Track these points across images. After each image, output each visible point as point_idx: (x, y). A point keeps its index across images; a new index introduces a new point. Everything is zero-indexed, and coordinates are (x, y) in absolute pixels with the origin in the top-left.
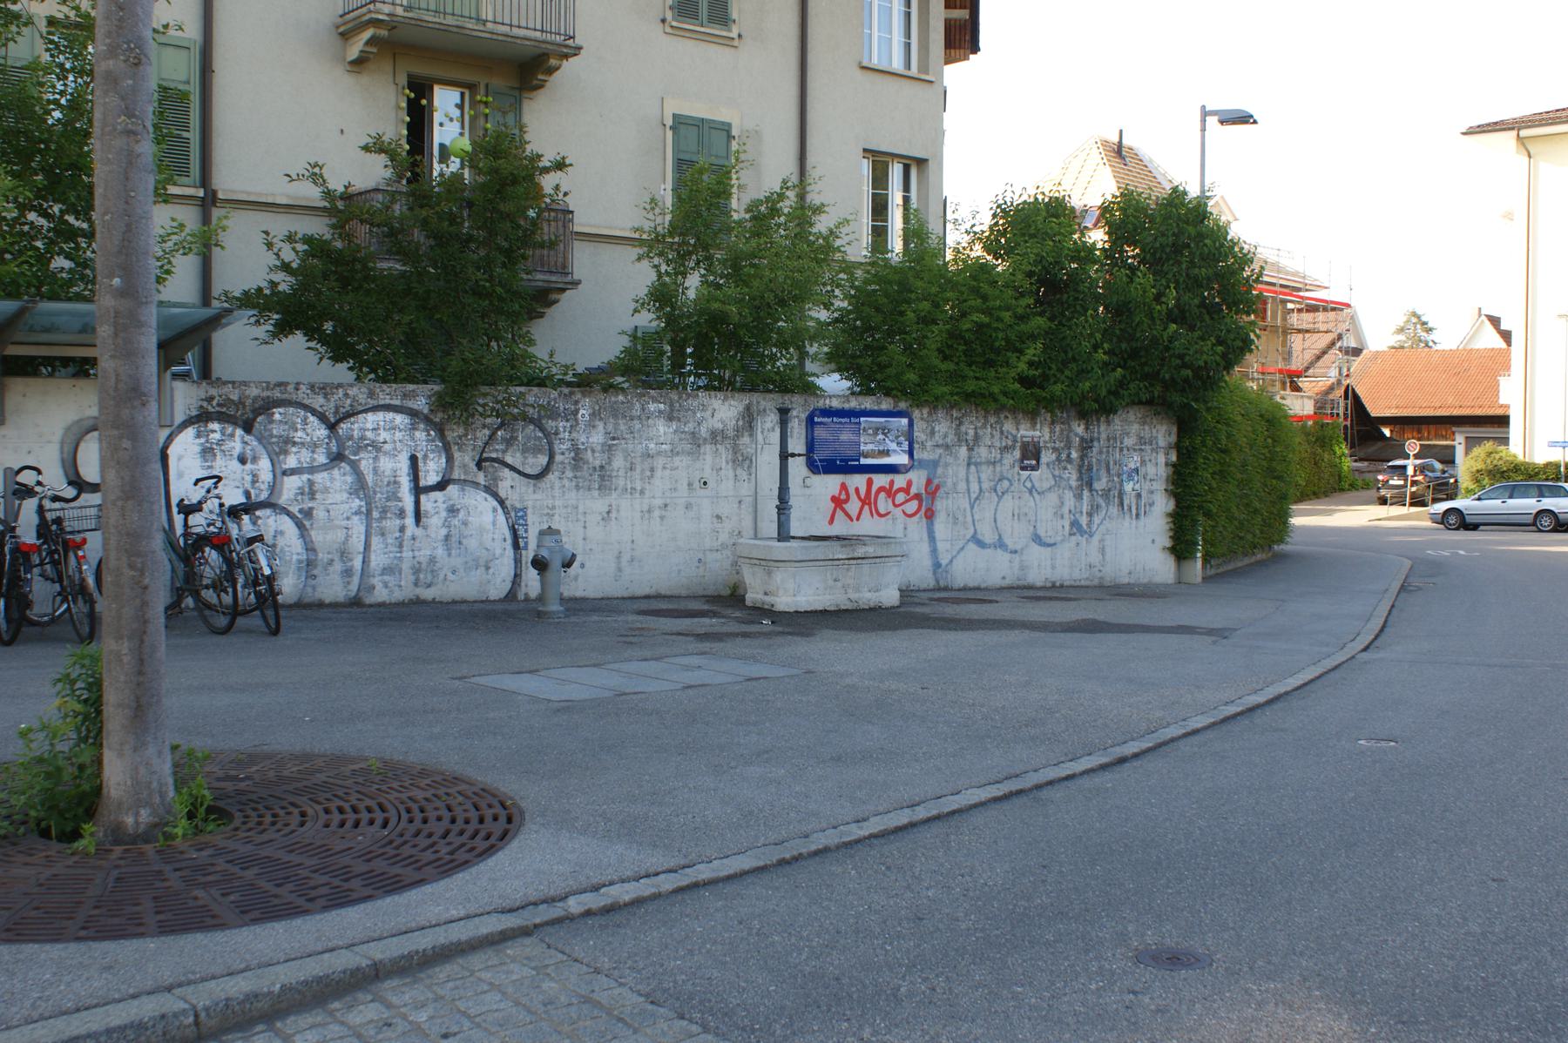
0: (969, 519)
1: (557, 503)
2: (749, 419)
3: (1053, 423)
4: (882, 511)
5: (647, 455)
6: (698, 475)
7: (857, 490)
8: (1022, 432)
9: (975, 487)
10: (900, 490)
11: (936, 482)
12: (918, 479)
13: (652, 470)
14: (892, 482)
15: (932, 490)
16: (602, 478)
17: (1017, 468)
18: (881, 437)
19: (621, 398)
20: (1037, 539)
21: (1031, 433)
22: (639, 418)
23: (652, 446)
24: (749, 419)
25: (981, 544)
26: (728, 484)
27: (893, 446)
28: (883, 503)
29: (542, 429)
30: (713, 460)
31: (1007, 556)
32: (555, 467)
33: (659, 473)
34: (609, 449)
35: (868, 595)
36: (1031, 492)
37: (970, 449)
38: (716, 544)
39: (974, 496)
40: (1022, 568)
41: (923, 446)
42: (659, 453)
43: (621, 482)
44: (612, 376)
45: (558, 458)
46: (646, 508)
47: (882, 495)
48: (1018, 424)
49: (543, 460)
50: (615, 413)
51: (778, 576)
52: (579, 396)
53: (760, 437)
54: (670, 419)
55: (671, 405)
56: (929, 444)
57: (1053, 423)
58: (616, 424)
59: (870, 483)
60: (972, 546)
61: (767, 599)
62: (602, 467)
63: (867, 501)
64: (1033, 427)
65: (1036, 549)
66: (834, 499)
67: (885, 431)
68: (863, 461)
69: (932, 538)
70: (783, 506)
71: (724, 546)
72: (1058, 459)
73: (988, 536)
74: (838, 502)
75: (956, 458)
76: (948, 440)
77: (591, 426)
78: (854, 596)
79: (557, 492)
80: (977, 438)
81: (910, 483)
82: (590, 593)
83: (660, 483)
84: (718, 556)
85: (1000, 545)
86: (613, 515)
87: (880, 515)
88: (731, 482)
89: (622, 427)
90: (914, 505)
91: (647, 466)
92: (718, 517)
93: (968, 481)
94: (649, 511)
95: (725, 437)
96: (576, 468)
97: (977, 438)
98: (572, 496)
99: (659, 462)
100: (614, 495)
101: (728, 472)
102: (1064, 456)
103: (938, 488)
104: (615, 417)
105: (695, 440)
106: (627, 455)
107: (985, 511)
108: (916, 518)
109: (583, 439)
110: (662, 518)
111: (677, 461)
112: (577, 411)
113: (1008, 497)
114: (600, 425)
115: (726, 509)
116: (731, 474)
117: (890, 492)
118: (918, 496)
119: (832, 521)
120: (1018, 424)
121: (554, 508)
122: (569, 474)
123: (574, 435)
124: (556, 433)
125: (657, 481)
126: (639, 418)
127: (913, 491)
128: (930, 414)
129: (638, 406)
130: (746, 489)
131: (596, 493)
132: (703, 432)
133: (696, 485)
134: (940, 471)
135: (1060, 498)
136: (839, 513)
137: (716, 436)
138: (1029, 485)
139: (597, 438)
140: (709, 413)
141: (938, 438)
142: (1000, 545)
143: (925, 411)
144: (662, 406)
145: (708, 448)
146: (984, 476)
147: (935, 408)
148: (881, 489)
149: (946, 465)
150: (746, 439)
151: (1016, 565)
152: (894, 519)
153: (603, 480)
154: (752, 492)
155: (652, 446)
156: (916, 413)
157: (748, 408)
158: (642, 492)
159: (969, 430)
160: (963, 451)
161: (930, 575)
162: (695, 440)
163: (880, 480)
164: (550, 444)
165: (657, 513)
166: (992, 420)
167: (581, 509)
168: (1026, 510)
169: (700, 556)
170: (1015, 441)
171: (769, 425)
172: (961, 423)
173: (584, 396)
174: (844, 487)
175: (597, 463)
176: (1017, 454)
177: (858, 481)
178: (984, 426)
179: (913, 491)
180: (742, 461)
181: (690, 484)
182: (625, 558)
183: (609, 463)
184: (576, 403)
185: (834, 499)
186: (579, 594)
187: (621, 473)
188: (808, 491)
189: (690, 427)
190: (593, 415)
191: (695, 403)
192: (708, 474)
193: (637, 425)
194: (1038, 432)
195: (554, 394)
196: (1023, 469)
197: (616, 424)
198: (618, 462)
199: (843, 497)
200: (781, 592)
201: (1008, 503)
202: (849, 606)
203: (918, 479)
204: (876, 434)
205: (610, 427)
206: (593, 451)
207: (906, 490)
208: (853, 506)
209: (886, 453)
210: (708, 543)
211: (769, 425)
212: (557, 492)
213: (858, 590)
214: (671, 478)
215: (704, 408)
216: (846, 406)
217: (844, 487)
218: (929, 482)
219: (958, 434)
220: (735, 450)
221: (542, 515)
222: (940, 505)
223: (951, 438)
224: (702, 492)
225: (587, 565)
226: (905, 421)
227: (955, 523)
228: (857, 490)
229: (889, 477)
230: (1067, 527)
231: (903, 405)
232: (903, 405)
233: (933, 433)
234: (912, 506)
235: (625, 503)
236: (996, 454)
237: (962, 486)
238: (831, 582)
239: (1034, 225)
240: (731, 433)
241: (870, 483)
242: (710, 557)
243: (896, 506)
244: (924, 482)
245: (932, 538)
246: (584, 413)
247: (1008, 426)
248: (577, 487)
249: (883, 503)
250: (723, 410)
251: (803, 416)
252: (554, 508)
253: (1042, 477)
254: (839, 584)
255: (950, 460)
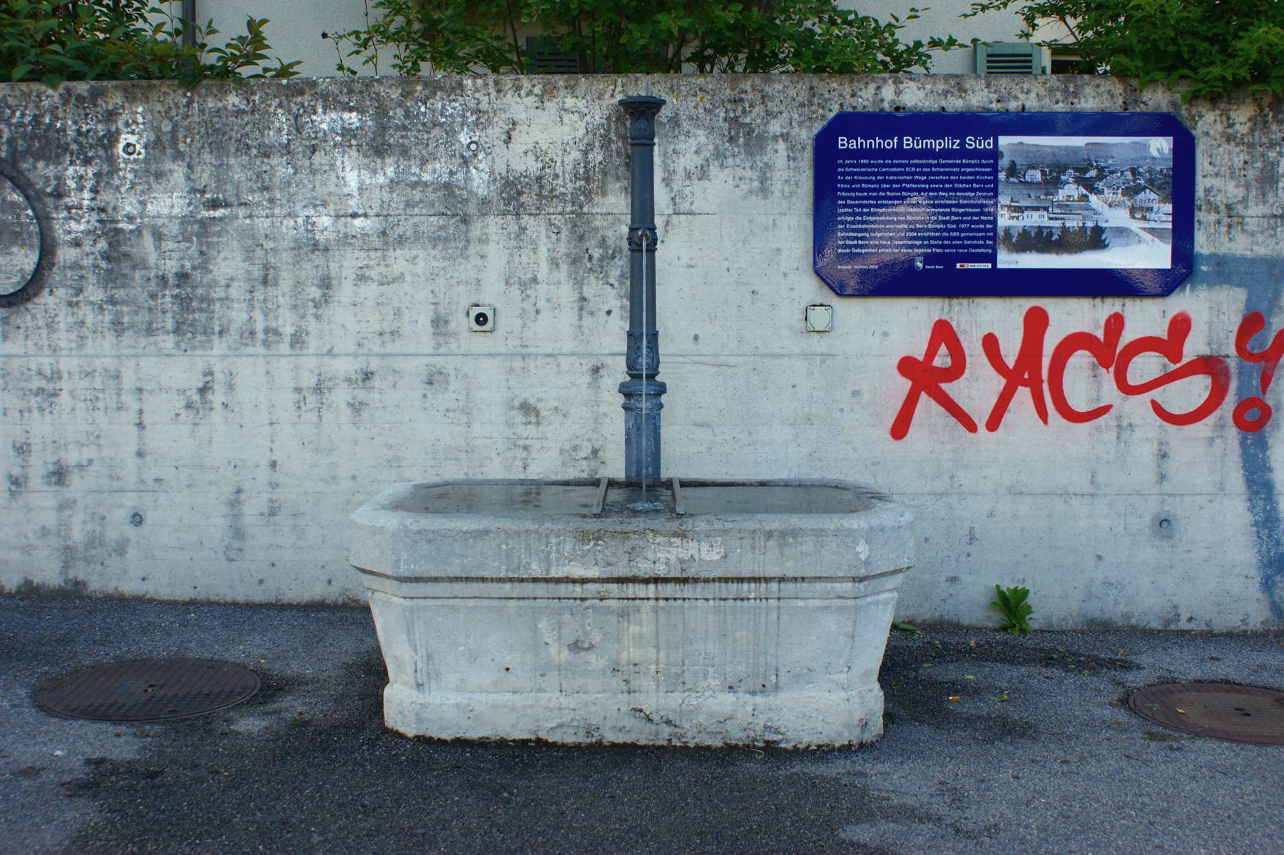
1: (66, 364)
4: (1079, 402)
5: (312, 246)
6: (463, 297)
7: (990, 344)
12: (1212, 315)
13: (326, 283)
14: (1115, 324)
16: (184, 303)
18: (1071, 191)
19: (233, 100)
22: (287, 149)
23: (325, 221)
27: (1117, 217)
28: (1083, 381)
29: (21, 185)
32: (56, 275)
33: (345, 291)
34: (200, 231)
35: (725, 702)
41: (1232, 216)
42: (346, 240)
43: (238, 315)
44: (105, 39)
45: (65, 255)
46: (309, 381)
47: (1081, 360)
49: (26, 259)
50: (217, 138)
52: (116, 99)
54: (378, 149)
55: (381, 113)
56: (1254, 211)
58: (221, 172)
59: (1036, 324)
62: (183, 277)
63: (1031, 373)
66: (907, 366)
67: (1090, 175)
68: (1007, 260)
74: (926, 377)
77: (152, 174)
78: (656, 700)
79: (64, 338)
81: (1181, 326)
82: (161, 588)
83: (348, 321)
86: (217, 397)
88: (568, 317)
89: (239, 175)
90: (1195, 390)
91: (309, 271)
92: (526, 408)
94: (318, 389)
96: (111, 279)
98: (105, 349)
99: (348, 263)
100: (219, 347)
104: (219, 148)
105: (456, 207)
106: (252, 244)
109: (129, 206)
110: (357, 407)
111: (399, 260)
112: (113, 138)
114: (178, 172)
115: (547, 386)
116: (566, 293)
117: (1109, 350)
118: (1209, 365)
119: (900, 429)
121: (56, 375)
122: (95, 293)
123: (106, 197)
124: (59, 194)
125: (340, 314)
126: (287, 149)
127: (1194, 347)
129: (282, 119)
131: (169, 342)
132: (479, 181)
133: (460, 323)
137: (514, 194)
139: (168, 204)
140: (496, 132)
143: (1242, 116)
144: (353, 118)
145: (493, 224)
153: (189, 306)
155: (325, 221)
156: (1207, 124)
158: (298, 340)
161: (1254, 590)
162: (456, 207)
163: (1071, 316)
164: (43, 220)
165: (341, 395)
167: (129, 379)
171: (688, 160)
173: (130, 97)
175: (171, 267)
179: (1194, 347)
181: (439, 323)
182: (252, 509)
183: (204, 267)
184: (111, 116)
185: (907, 366)
186: (131, 586)
187: (237, 291)
188: (819, 345)
189: (438, 170)
190: (156, 146)
191: (454, 108)
192: (492, 295)
193: (281, 168)
195: (51, 96)
197: (221, 172)
198: (229, 264)
199: (942, 359)
202: (641, 734)
203: (1212, 315)
204: (1052, 183)
205: (204, 176)
206: (158, 237)
207: (1171, 344)
208: (978, 388)
209: (1096, 239)
212: (64, 338)
213: (676, 680)
214: (387, 302)
215: (481, 118)
216: (955, 104)
217: (943, 333)
218: (1252, 323)
221: (25, 393)
224: (481, 343)
225: (150, 517)
226: (1160, 146)
229: (1109, 306)
231: (1157, 99)
232: (1157, 99)
235: (249, 369)
240: (566, 185)
241: (1036, 324)
244: (1233, 321)
246: (132, 140)
248: (118, 327)
249: (1083, 381)
251: (806, 135)
252: (56, 375)
254: (596, 661)
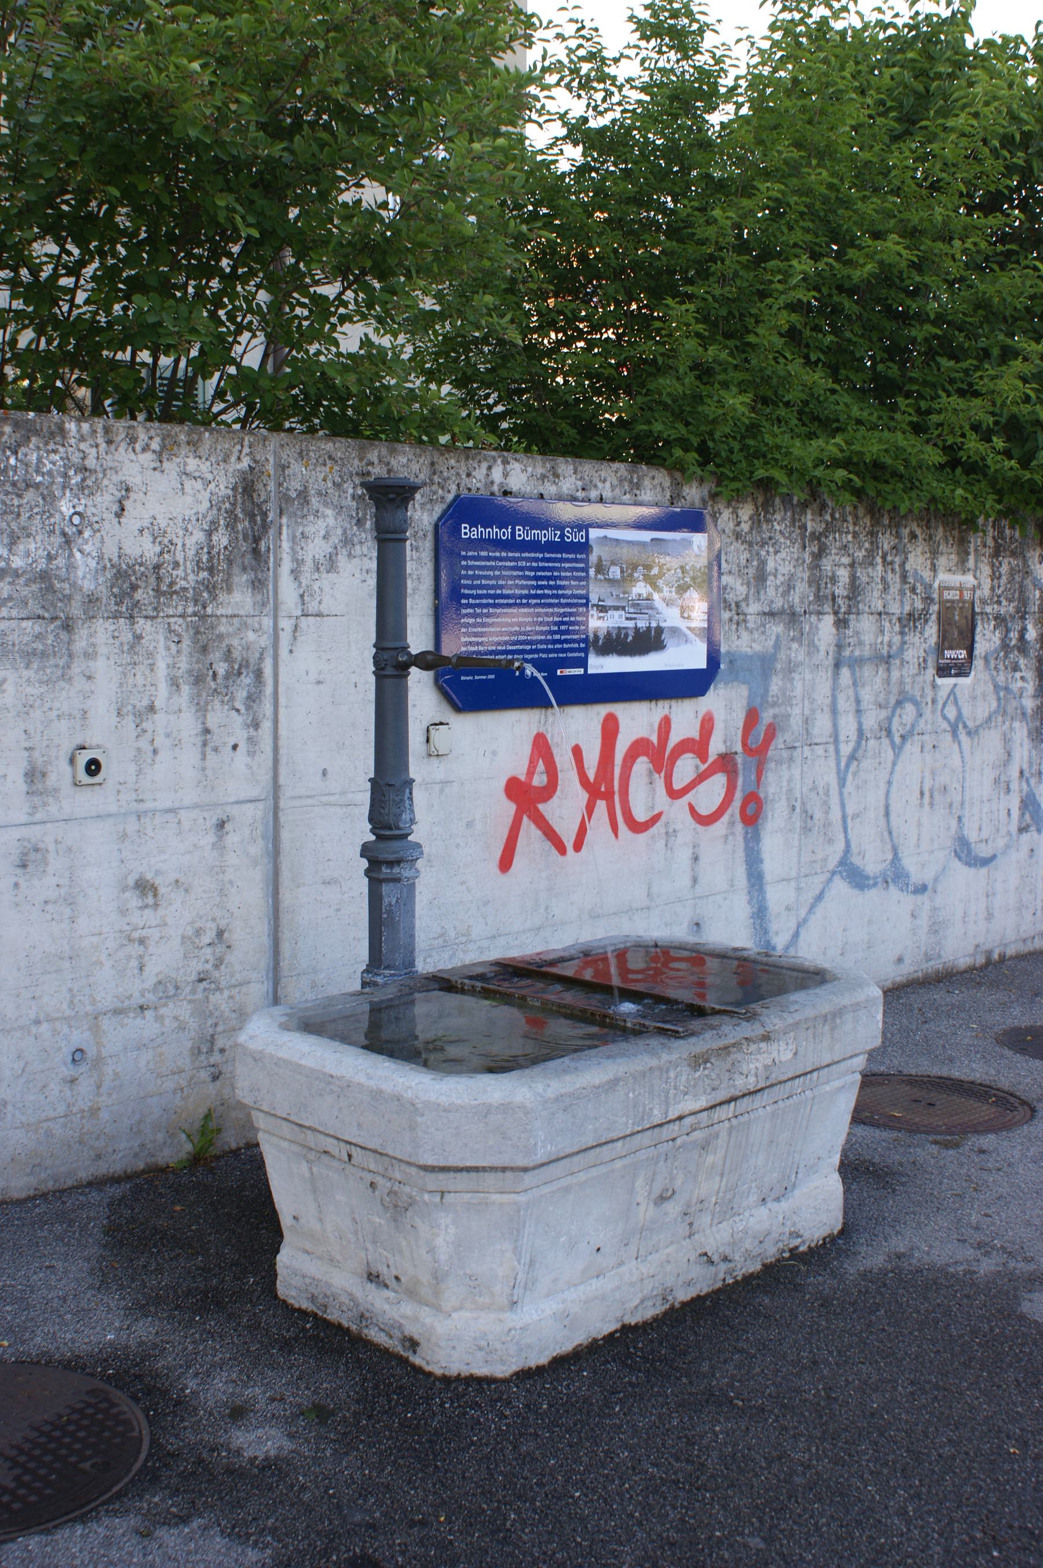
0: (836, 815)
2: (250, 522)
3: (997, 553)
4: (641, 815)
7: (577, 751)
8: (943, 577)
9: (848, 726)
10: (685, 746)
11: (766, 717)
14: (665, 725)
15: (760, 739)
17: (931, 671)
20: (965, 852)
21: (956, 579)
24: (250, 522)
25: (858, 879)
26: (179, 770)
30: (118, 682)
31: (909, 901)
36: (954, 733)
37: (841, 623)
38: (137, 987)
39: (846, 750)
40: (936, 928)
48: (934, 553)
51: (440, 1233)
53: (288, 591)
56: (753, 608)
57: (997, 553)
59: (610, 729)
60: (840, 886)
61: (381, 1303)
64: (962, 565)
65: (962, 875)
66: (516, 789)
68: (601, 665)
69: (756, 878)
70: (388, 852)
71: (167, 989)
72: (1005, 646)
73: (872, 860)
74: (526, 797)
75: (812, 648)
76: (795, 598)
78: (715, 1237)
80: (855, 590)
81: (707, 725)
84: (146, 1027)
85: (895, 875)
87: (637, 827)
88: (190, 756)
92: (145, 887)
93: (834, 711)
95: (166, 592)
97: (855, 590)
101: (177, 718)
102: (1014, 635)
103: (771, 732)
107: (865, 797)
108: (720, 827)
113: (911, 748)
115: (170, 854)
116: (188, 724)
118: (726, 763)
120: (934, 553)
127: (716, 747)
128: (756, 522)
130: (241, 778)
132: (85, 570)
133: (60, 774)
134: (776, 685)
135: (1006, 740)
136: (529, 830)
137: (131, 588)
138: (951, 713)
140: (105, 501)
141: (772, 591)
142: (895, 875)
145: (101, 634)
146: (867, 695)
147: (767, 506)
148: (639, 748)
149: (791, 668)
150: (239, 599)
151: (924, 922)
152: (670, 835)
154: (261, 788)
157: (247, 486)
159: (838, 568)
160: (826, 628)
163: (637, 720)
166: (886, 541)
168: (943, 778)
169: (79, 1037)
170: (928, 600)
171: (316, 549)
172: (821, 553)
174: (541, 747)
176: (932, 631)
177: (577, 726)
178: (869, 561)
179: (716, 747)
180: (229, 677)
181: (34, 775)
191: (52, 462)
192: (103, 733)
194: (961, 577)
196: (943, 671)
199: (540, 780)
200: (452, 1293)
201: (913, 763)
207: (698, 747)
208: (565, 808)
210: (108, 986)
211: (316, 549)
217: (541, 747)
218: (752, 717)
219: (815, 582)
220: (203, 637)
222: (779, 783)
223: (802, 589)
227: (806, 830)
228: (577, 751)
230: (1016, 813)
233: (761, 577)
234: (711, 794)
236: (891, 634)
237: (822, 725)
238: (646, 1211)
239: (661, 143)
240: (187, 578)
241: (610, 729)
242: (117, 1035)
243: (674, 794)
245: (756, 878)
247: (917, 560)
249: (644, 793)
250: (159, 493)
253: (973, 690)
254: (673, 1208)
255: (797, 652)
